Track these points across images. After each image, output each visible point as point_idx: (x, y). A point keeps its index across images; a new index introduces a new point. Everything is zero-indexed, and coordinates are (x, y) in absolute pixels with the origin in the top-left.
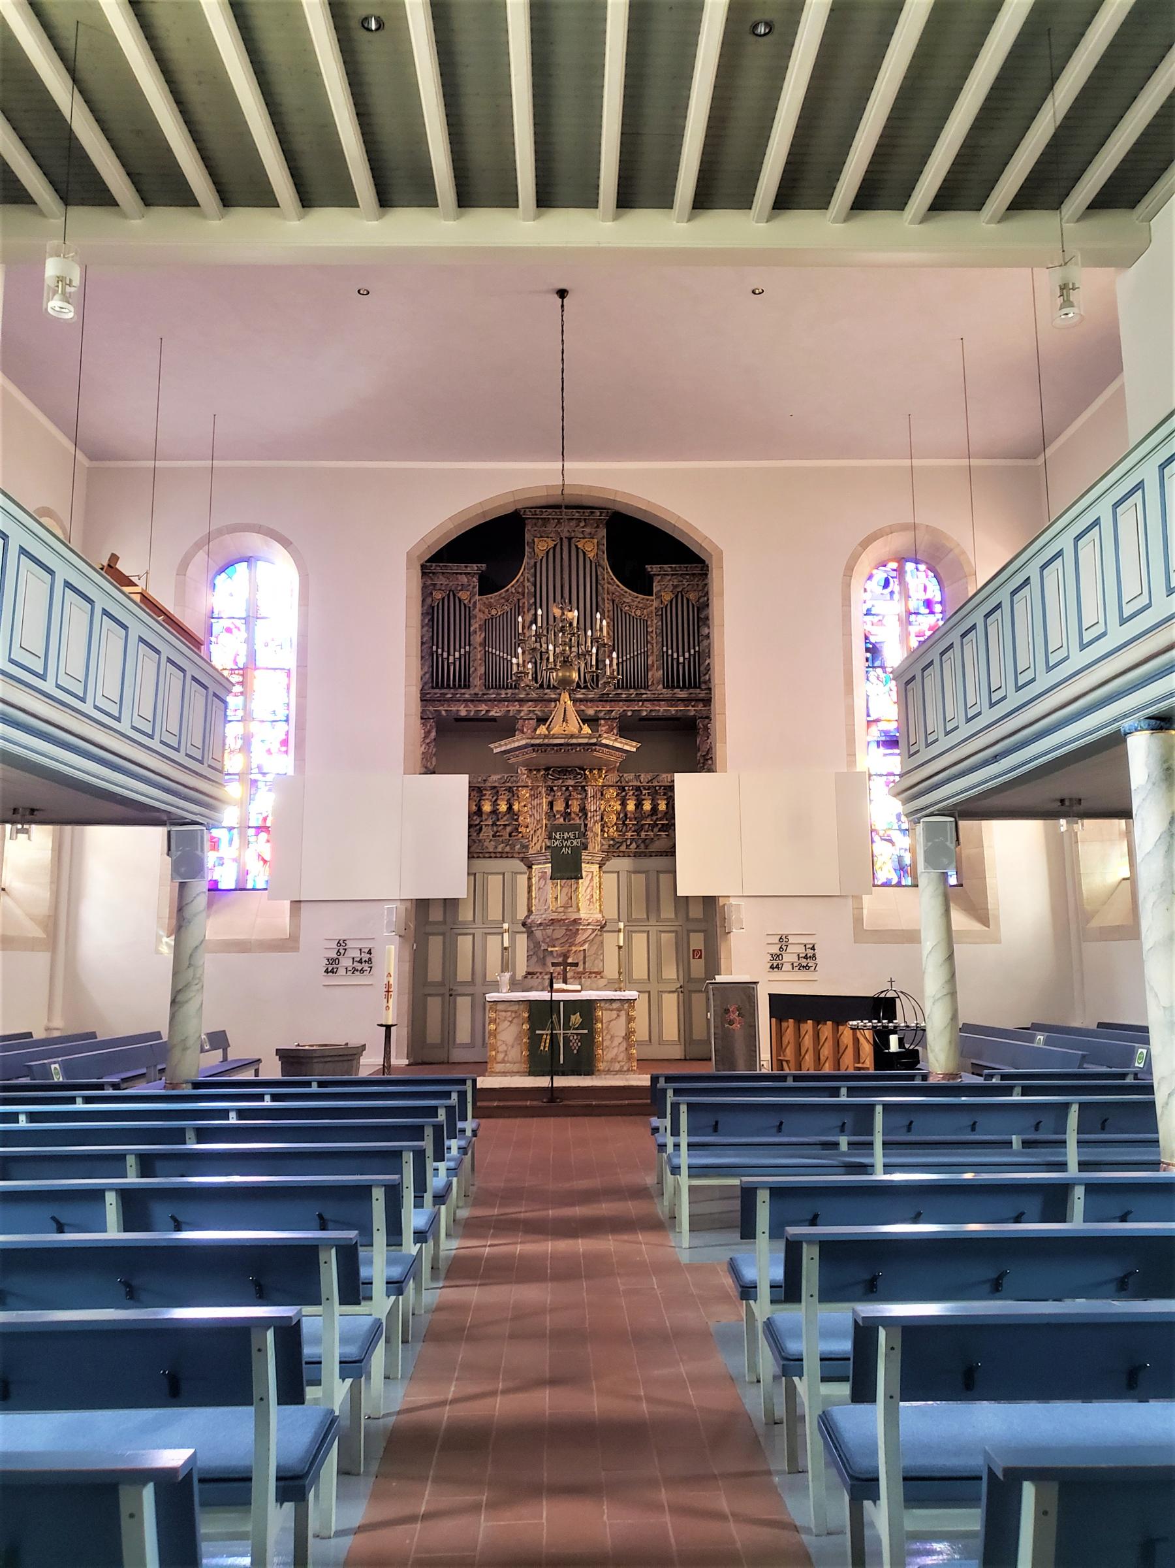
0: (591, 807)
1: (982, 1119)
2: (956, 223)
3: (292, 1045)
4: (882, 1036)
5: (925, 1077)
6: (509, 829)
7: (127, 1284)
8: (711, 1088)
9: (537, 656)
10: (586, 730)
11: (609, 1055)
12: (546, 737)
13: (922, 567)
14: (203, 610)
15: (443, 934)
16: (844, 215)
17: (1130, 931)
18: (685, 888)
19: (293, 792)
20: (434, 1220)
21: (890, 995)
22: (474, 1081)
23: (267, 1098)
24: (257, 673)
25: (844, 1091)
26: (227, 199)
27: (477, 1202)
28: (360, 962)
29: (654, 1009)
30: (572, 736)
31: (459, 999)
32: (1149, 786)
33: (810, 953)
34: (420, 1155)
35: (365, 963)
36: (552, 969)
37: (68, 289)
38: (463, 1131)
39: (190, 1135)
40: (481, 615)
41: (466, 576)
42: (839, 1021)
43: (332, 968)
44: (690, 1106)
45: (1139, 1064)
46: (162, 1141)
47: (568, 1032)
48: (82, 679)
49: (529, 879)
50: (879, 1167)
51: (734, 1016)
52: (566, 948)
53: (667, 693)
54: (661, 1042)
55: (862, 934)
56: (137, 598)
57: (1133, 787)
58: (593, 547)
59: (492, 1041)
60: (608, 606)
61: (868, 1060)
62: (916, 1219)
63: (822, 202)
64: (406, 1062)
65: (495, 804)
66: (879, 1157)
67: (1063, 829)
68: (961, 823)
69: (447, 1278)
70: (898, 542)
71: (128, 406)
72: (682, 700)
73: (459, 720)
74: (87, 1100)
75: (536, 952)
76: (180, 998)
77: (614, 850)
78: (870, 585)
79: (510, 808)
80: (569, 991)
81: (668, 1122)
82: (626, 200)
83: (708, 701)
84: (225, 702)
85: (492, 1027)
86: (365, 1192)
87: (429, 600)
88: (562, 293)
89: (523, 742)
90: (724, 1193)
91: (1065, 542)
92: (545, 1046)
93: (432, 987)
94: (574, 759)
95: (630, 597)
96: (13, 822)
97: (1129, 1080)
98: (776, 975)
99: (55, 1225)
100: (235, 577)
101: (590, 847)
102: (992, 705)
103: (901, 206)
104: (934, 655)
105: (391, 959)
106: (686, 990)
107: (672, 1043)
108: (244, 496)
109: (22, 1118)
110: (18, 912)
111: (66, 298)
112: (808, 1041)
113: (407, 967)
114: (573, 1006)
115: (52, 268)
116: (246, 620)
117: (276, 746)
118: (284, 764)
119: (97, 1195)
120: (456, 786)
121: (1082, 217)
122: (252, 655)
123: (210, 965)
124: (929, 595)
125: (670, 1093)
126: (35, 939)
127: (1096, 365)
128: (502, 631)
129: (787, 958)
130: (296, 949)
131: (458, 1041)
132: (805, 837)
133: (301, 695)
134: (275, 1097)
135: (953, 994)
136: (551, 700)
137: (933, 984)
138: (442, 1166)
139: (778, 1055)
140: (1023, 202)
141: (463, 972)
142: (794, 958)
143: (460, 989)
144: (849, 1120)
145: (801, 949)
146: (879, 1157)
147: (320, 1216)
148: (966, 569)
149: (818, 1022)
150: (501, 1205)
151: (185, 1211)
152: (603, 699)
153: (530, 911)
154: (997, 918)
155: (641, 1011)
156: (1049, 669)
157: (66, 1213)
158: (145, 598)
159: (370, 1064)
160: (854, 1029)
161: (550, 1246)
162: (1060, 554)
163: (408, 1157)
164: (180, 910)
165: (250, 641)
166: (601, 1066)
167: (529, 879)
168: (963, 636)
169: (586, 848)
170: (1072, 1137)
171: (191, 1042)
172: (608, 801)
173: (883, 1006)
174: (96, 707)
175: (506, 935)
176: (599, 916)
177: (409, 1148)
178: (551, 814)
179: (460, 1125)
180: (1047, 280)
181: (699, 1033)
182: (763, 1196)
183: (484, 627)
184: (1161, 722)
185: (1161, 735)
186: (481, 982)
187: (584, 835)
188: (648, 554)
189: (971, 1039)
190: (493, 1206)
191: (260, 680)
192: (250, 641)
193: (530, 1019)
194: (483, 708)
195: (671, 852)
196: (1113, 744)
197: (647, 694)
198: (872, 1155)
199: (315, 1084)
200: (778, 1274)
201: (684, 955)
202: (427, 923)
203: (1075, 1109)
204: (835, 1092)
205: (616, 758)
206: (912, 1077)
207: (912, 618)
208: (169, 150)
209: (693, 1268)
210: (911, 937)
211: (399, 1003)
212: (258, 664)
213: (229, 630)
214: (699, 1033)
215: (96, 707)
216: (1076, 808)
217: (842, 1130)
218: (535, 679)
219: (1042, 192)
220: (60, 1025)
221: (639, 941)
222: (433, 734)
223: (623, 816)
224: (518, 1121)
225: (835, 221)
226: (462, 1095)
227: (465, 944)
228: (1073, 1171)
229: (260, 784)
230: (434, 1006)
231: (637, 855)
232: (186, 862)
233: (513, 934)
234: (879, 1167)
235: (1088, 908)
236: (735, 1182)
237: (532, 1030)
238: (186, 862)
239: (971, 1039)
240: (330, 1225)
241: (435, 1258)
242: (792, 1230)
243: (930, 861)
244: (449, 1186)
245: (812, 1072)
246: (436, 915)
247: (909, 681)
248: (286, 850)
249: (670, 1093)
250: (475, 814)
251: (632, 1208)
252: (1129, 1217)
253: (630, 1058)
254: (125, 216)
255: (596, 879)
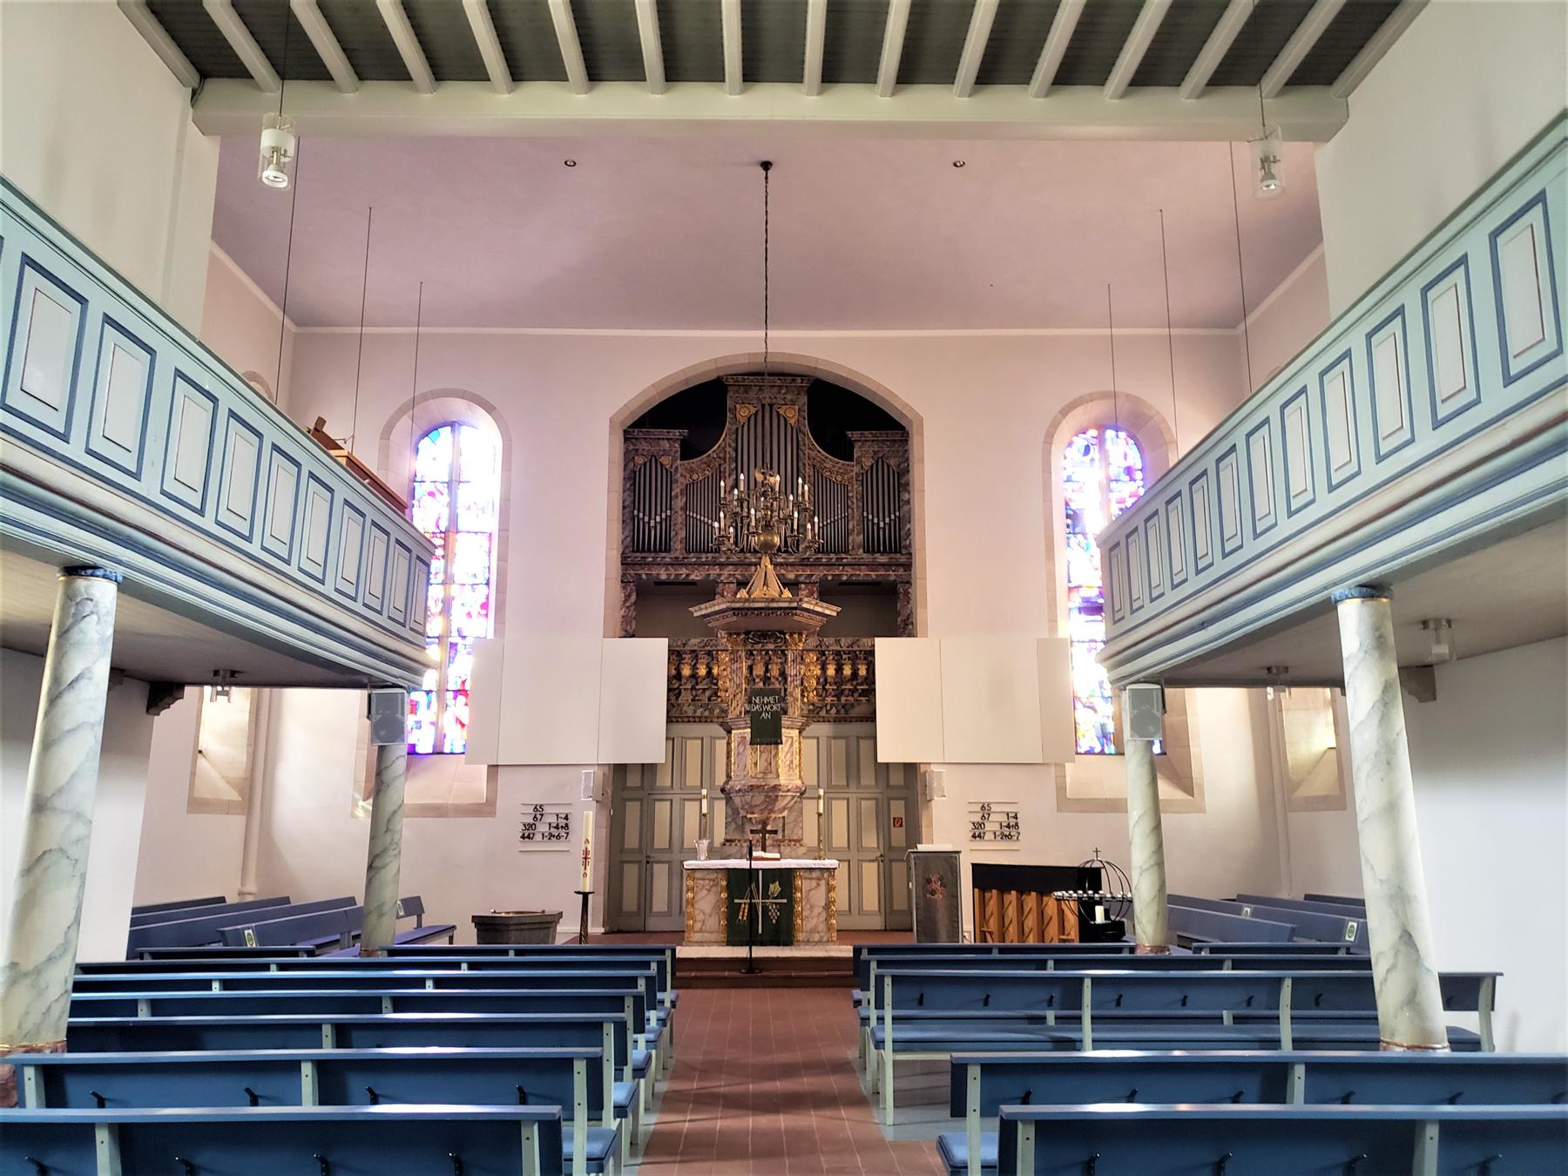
0: (791, 671)
1: (1194, 994)
2: (1156, 99)
3: (486, 912)
4: (1087, 907)
5: (1132, 950)
6: (708, 693)
7: (323, 1160)
8: (914, 958)
9: (738, 520)
10: (787, 594)
11: (808, 925)
12: (747, 600)
13: (1122, 435)
14: (407, 475)
15: (641, 800)
16: (1120, 92)
17: (1339, 799)
18: (882, 758)
19: (492, 657)
20: (634, 1095)
21: (1096, 865)
22: (674, 951)
23: (464, 966)
24: (459, 536)
25: (1051, 964)
26: (439, 73)
27: (675, 1076)
28: (557, 827)
29: (855, 878)
30: (773, 600)
31: (656, 866)
32: (1361, 655)
33: (1012, 822)
34: (621, 1027)
35: (562, 828)
36: (751, 837)
37: (283, 159)
38: (662, 1002)
39: (386, 1004)
40: (682, 480)
41: (668, 442)
42: (1044, 892)
43: (528, 833)
44: (896, 980)
45: (1350, 938)
46: (357, 1012)
47: (768, 901)
48: (287, 541)
49: (729, 744)
50: (1088, 1042)
51: (937, 886)
52: (765, 815)
53: (867, 558)
54: (861, 911)
55: (1064, 802)
56: (343, 461)
57: (1345, 655)
58: (794, 413)
59: (690, 909)
60: (809, 471)
61: (1073, 931)
62: (1131, 1098)
63: (1025, 78)
64: (602, 930)
65: (694, 667)
66: (1087, 1032)
67: (1270, 697)
68: (1167, 691)
69: (646, 1154)
70: (1098, 409)
71: (336, 275)
72: (883, 565)
73: (660, 583)
74: (282, 967)
75: (736, 819)
76: (377, 863)
77: (814, 714)
78: (1069, 452)
79: (709, 672)
80: (768, 860)
81: (871, 994)
82: (832, 74)
83: (908, 566)
84: (428, 565)
85: (690, 895)
86: (566, 1064)
87: (631, 465)
88: (766, 166)
89: (724, 606)
90: (929, 1069)
91: (1272, 410)
92: (743, 915)
93: (629, 855)
94: (772, 623)
95: (831, 462)
96: (213, 684)
97: (1342, 955)
98: (978, 844)
99: (248, 1097)
100: (438, 441)
101: (790, 711)
102: (1198, 572)
103: (1102, 82)
104: (1139, 521)
105: (588, 825)
106: (886, 860)
107: (871, 913)
108: (446, 366)
109: (216, 985)
110: (214, 774)
111: (281, 168)
112: (1011, 912)
113: (604, 832)
114: (772, 875)
115: (268, 139)
116: (449, 484)
117: (476, 609)
118: (483, 627)
119: (293, 1066)
120: (655, 650)
121: (1280, 93)
122: (453, 519)
123: (408, 830)
124: (1130, 463)
125: (873, 965)
126: (230, 802)
127: (1296, 235)
128: (705, 496)
129: (989, 827)
130: (492, 814)
131: (655, 909)
132: (1013, 703)
133: (502, 558)
134: (472, 966)
135: (1160, 864)
136: (751, 564)
137: (1140, 854)
138: (641, 1038)
139: (981, 925)
140: (1224, 77)
141: (661, 841)
142: (997, 827)
143: (658, 857)
144: (1057, 994)
145: (1004, 818)
146: (1087, 1032)
147: (520, 1089)
148: (1167, 437)
149: (1021, 892)
150: (700, 1079)
151: (382, 1083)
152: (804, 563)
153: (729, 777)
154: (1201, 787)
155: (841, 880)
156: (1256, 536)
157: (261, 1085)
158: (351, 461)
159: (567, 931)
160: (1058, 900)
161: (751, 1122)
162: (1266, 421)
163: (609, 1029)
164: (379, 774)
165: (452, 506)
166: (801, 936)
167: (729, 744)
168: (1169, 502)
169: (785, 713)
170: (1285, 1013)
171: (386, 908)
172: (808, 665)
173: (1087, 877)
174: (300, 570)
175: (704, 802)
176: (799, 783)
177: (610, 1020)
178: (750, 679)
179: (660, 996)
180: (1247, 154)
181: (900, 903)
182: (974, 1074)
183: (685, 491)
184: (1372, 590)
185: (1371, 603)
186: (678, 850)
187: (784, 700)
188: (849, 421)
189: (1179, 911)
190: (692, 1079)
191: (461, 543)
192: (452, 506)
193: (729, 888)
194: (684, 571)
195: (871, 718)
196: (1325, 610)
197: (847, 559)
198: (1081, 1030)
199: (512, 953)
200: (992, 1153)
201: (885, 823)
202: (624, 788)
203: (1288, 984)
204: (1042, 965)
205: (816, 622)
206: (1119, 950)
207: (1113, 485)
208: (385, 26)
209: (896, 1146)
210: (1116, 806)
211: (595, 870)
212: (460, 527)
213: (431, 494)
214: (900, 903)
215: (300, 570)
216: (1283, 676)
217: (1050, 1003)
218: (736, 543)
219: (1240, 69)
220: (253, 889)
221: (839, 808)
222: (634, 598)
223: (823, 680)
224: (716, 992)
225: (1037, 96)
226: (662, 965)
227: (662, 809)
228: (1287, 1050)
229: (460, 648)
230: (631, 873)
231: (837, 720)
232: (386, 725)
233: (711, 800)
234: (1088, 1042)
235: (1294, 778)
236: (945, 1057)
237: (730, 898)
238: (386, 725)
239: (1177, 909)
240: (530, 1098)
241: (634, 1135)
242: (1007, 1109)
243: (1139, 727)
244: (649, 1057)
245: (1016, 944)
246: (633, 780)
247: (1116, 548)
248: (493, 710)
249: (873, 965)
250: (674, 678)
251: (834, 1083)
252: (1352, 1098)
253: (829, 928)
254: (339, 90)
255: (796, 745)
